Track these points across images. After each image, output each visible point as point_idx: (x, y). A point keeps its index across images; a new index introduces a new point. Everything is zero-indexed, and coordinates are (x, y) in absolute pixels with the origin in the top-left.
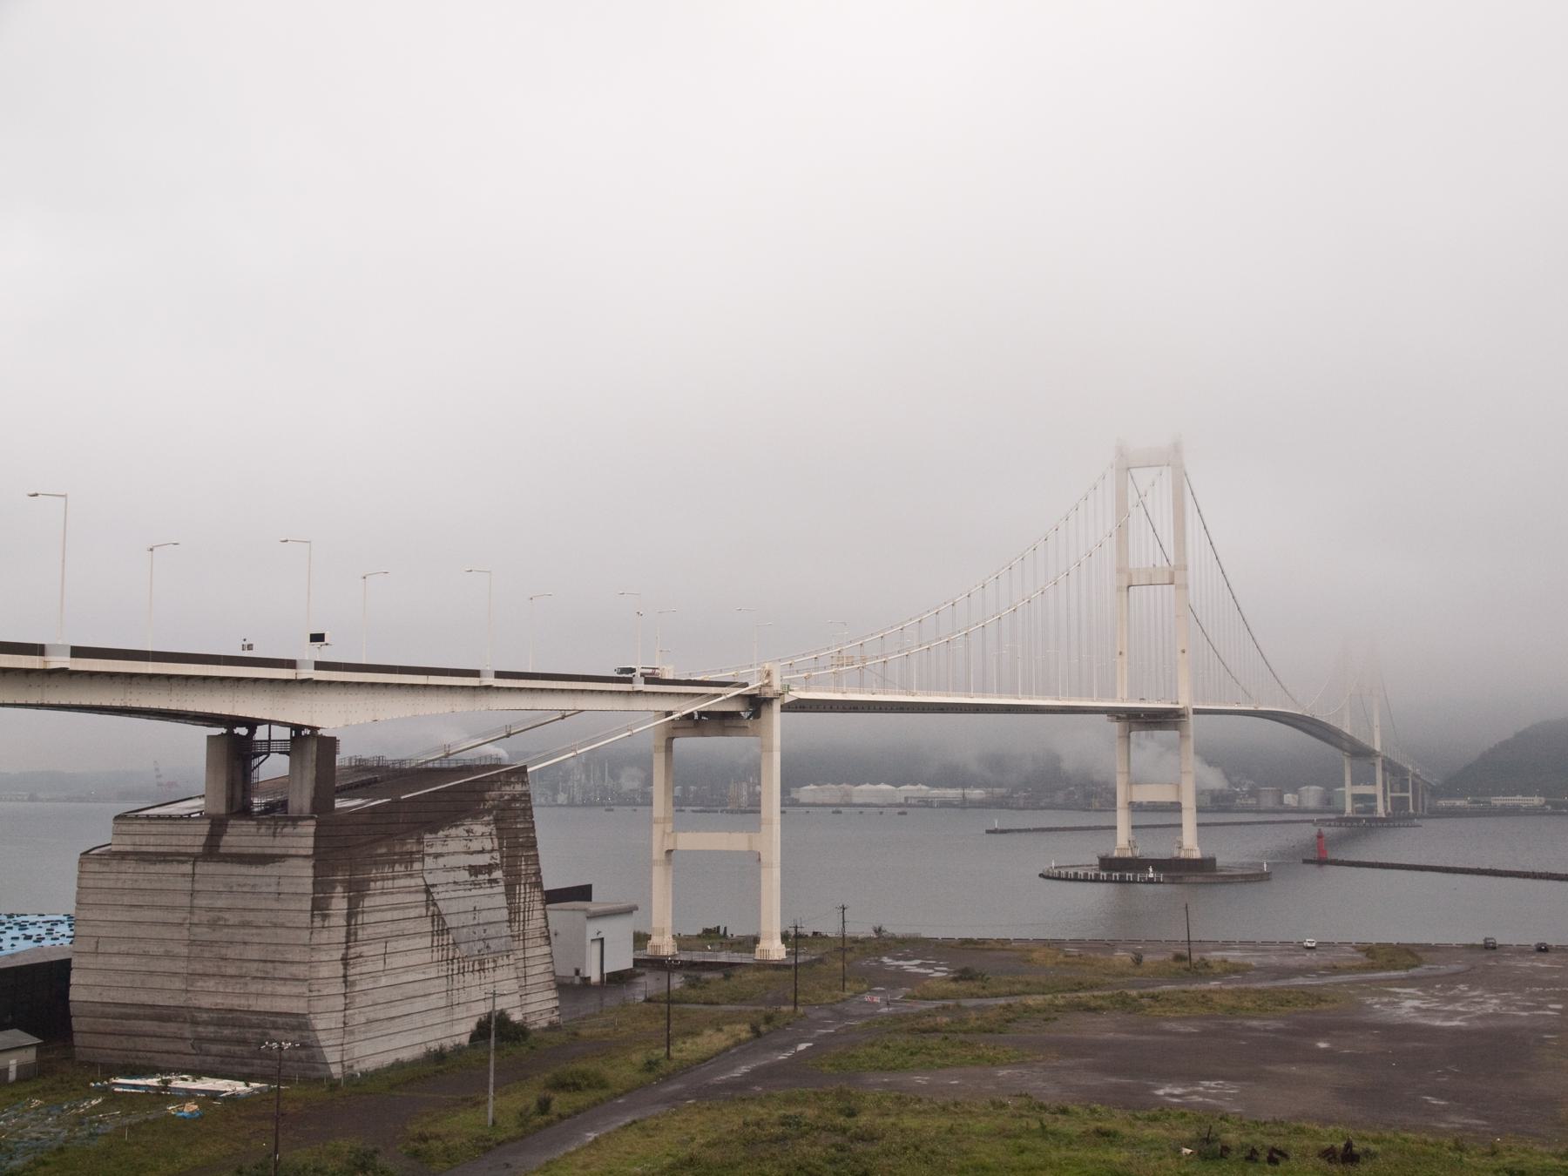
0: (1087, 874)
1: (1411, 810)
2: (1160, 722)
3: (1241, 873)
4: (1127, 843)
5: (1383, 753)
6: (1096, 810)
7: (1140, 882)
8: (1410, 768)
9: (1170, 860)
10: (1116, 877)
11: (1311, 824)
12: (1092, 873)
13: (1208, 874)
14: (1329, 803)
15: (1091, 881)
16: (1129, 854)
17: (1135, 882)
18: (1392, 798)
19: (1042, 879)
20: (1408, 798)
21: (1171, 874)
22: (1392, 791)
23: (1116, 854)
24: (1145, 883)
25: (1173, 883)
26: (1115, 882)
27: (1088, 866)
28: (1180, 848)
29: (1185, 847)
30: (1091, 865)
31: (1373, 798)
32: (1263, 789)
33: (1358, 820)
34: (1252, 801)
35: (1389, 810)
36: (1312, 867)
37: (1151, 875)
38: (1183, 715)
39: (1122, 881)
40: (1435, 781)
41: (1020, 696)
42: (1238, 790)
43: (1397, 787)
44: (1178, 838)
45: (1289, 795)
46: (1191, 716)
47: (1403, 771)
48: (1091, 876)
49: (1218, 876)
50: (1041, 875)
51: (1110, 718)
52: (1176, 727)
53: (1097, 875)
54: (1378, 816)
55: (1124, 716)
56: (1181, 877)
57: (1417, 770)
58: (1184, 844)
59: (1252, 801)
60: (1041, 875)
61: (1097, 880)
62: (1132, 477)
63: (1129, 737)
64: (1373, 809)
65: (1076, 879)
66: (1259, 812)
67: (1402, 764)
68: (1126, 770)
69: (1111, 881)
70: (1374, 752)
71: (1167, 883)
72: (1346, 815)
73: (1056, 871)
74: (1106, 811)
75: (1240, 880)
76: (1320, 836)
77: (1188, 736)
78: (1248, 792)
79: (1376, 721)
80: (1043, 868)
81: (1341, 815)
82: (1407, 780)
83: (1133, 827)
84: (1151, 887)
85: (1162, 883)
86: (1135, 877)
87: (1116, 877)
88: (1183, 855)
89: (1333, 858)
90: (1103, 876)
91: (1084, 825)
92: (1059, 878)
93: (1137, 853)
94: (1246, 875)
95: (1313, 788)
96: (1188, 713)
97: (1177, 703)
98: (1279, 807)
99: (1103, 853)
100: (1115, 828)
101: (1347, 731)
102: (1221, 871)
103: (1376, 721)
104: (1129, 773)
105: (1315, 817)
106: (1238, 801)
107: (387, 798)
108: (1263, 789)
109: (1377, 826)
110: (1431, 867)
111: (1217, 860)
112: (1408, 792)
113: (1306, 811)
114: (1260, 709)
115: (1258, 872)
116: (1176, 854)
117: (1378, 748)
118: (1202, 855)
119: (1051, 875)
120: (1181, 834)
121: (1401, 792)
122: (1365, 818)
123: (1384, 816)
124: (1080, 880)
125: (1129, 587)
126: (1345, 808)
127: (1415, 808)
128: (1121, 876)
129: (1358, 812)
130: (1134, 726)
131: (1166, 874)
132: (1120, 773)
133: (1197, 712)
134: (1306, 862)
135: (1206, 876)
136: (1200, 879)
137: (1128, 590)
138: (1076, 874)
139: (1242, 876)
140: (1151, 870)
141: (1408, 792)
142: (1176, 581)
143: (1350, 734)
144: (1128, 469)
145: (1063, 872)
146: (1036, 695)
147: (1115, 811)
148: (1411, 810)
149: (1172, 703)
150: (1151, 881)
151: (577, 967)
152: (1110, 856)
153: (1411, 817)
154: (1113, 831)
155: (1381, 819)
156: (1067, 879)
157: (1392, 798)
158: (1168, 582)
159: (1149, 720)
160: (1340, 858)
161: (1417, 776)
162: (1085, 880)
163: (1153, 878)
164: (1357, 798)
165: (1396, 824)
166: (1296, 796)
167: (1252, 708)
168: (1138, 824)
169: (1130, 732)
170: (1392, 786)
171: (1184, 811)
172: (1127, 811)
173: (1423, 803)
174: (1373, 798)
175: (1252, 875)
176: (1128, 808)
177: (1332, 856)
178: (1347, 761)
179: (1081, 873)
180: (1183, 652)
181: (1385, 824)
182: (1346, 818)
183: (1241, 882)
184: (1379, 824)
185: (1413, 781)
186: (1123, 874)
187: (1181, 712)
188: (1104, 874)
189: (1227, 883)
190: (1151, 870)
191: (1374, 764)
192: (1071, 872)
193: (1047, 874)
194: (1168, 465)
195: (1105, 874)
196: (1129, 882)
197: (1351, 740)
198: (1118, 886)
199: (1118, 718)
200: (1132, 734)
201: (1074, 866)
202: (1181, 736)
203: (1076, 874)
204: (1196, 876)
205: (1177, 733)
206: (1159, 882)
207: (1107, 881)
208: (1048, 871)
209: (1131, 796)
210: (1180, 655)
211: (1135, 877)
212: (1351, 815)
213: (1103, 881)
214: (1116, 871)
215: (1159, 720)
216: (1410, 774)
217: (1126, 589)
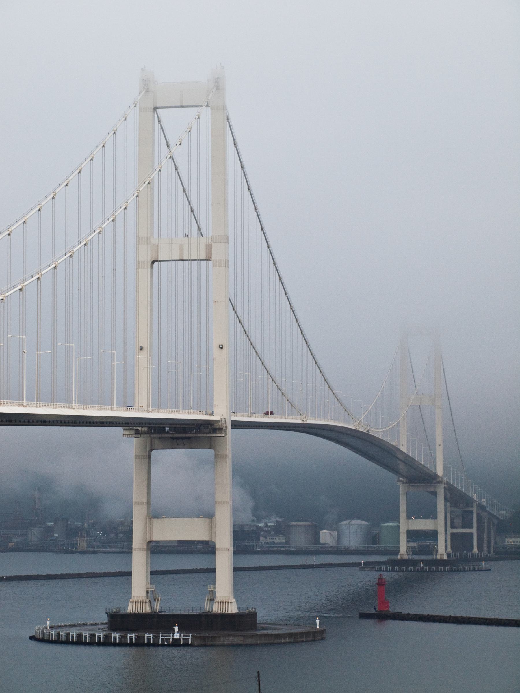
0: (94, 636)
1: (475, 550)
2: (189, 438)
3: (289, 632)
4: (144, 594)
5: (446, 479)
6: (83, 552)
7: (163, 645)
8: (475, 497)
9: (199, 616)
10: (131, 639)
11: (357, 568)
12: (100, 635)
13: (249, 633)
14: (374, 542)
15: (99, 644)
16: (147, 609)
17: (156, 644)
18: (453, 535)
19: (34, 643)
20: (472, 534)
21: (202, 635)
22: (453, 527)
23: (130, 609)
24: (169, 645)
25: (205, 646)
26: (131, 645)
27: (92, 624)
28: (212, 600)
29: (218, 599)
30: (96, 624)
31: (433, 535)
32: (295, 523)
33: (414, 563)
34: (280, 540)
35: (449, 550)
36: (370, 623)
37: (177, 636)
38: (220, 429)
39: (139, 644)
40: (502, 514)
41: (181, 411)
42: (262, 525)
43: (458, 521)
44: (209, 588)
45: (325, 531)
46: (229, 429)
47: (469, 501)
48: (99, 638)
49: (261, 636)
50: (32, 638)
51: (127, 432)
52: (210, 444)
53: (107, 637)
54: (438, 557)
55: (145, 429)
56: (214, 637)
57: (483, 500)
58: (218, 595)
59: (280, 540)
60: (32, 638)
61: (107, 643)
62: (159, 121)
63: (149, 457)
64: (432, 550)
65: (79, 642)
66: (288, 553)
67: (467, 492)
68: (145, 500)
69: (126, 645)
70: (436, 476)
71: (198, 646)
72: (399, 557)
73: (53, 632)
74: (94, 552)
75: (287, 640)
76: (381, 583)
77: (225, 457)
78: (274, 528)
79: (439, 440)
80: (36, 629)
81: (393, 557)
82: (472, 512)
83: (153, 573)
84: (175, 652)
85: (192, 645)
86: (156, 637)
87: (131, 639)
88: (215, 609)
89: (396, 611)
90: (115, 638)
91: (44, 572)
92: (57, 642)
93: (157, 607)
94: (296, 634)
95: (356, 522)
96: (226, 427)
97: (213, 414)
98: (315, 548)
99: (114, 608)
100: (130, 574)
101: (404, 449)
102: (263, 629)
103: (439, 440)
104: (148, 503)
105: (362, 559)
106: (262, 539)
107: (385, 526)
108: (295, 523)
109: (430, 571)
110: (486, 619)
111: (258, 614)
112: (472, 527)
113: (347, 552)
114: (308, 422)
115: (309, 630)
116: (206, 608)
117: (440, 472)
118: (239, 608)
119: (46, 638)
120: (214, 582)
121: (463, 527)
122: (422, 561)
123: (445, 557)
124: (85, 644)
125: (153, 262)
126: (398, 548)
127: (480, 547)
128: (137, 638)
129: (414, 553)
130: (156, 442)
131: (154, 634)
132: (138, 503)
133: (236, 425)
134: (363, 616)
135: (247, 637)
136: (237, 640)
137: (152, 268)
138: (80, 635)
139: (290, 635)
140: (176, 629)
141: (472, 527)
142: (213, 258)
143: (406, 453)
144: (155, 109)
145: (62, 633)
146: (311, 416)
147: (132, 552)
148: (475, 550)
149: (206, 414)
150: (176, 643)
151: (259, 671)
152: (122, 612)
153: (480, 559)
154: (211, 574)
155: (442, 562)
156: (67, 642)
157: (453, 535)
158: (204, 258)
159: (176, 435)
160: (405, 612)
161: (481, 507)
162: (92, 643)
163: (179, 640)
164: (412, 535)
165: (461, 568)
166: (335, 533)
167: (299, 421)
168: (241, 566)
169: (151, 450)
170: (452, 522)
171: (217, 552)
172: (145, 552)
173: (489, 542)
174: (433, 535)
175: (302, 634)
176: (148, 549)
177: (394, 608)
178: (402, 489)
179: (86, 634)
180: (221, 347)
181: (448, 568)
182: (399, 560)
183: (290, 643)
184: (433, 568)
185: (478, 515)
186: (140, 634)
187: (216, 425)
188: (116, 636)
189: (273, 644)
190: (176, 629)
191: (435, 494)
192: (74, 633)
193: (40, 637)
194: (207, 106)
195: (117, 635)
196: (149, 645)
197: (408, 461)
198: (133, 651)
199: (137, 432)
200: (154, 452)
201: (75, 626)
202: (216, 456)
203: (80, 635)
204: (234, 636)
205: (212, 451)
206: (186, 645)
207: (120, 645)
208: (43, 633)
209: (409, 527)
210: (217, 352)
211: (156, 637)
212: (406, 557)
213: (115, 644)
214: (132, 631)
215: (188, 435)
216: (475, 504)
217: (149, 264)
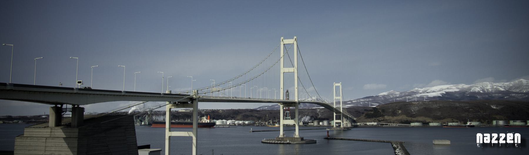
120: (295, 132)
164: (336, 123)
